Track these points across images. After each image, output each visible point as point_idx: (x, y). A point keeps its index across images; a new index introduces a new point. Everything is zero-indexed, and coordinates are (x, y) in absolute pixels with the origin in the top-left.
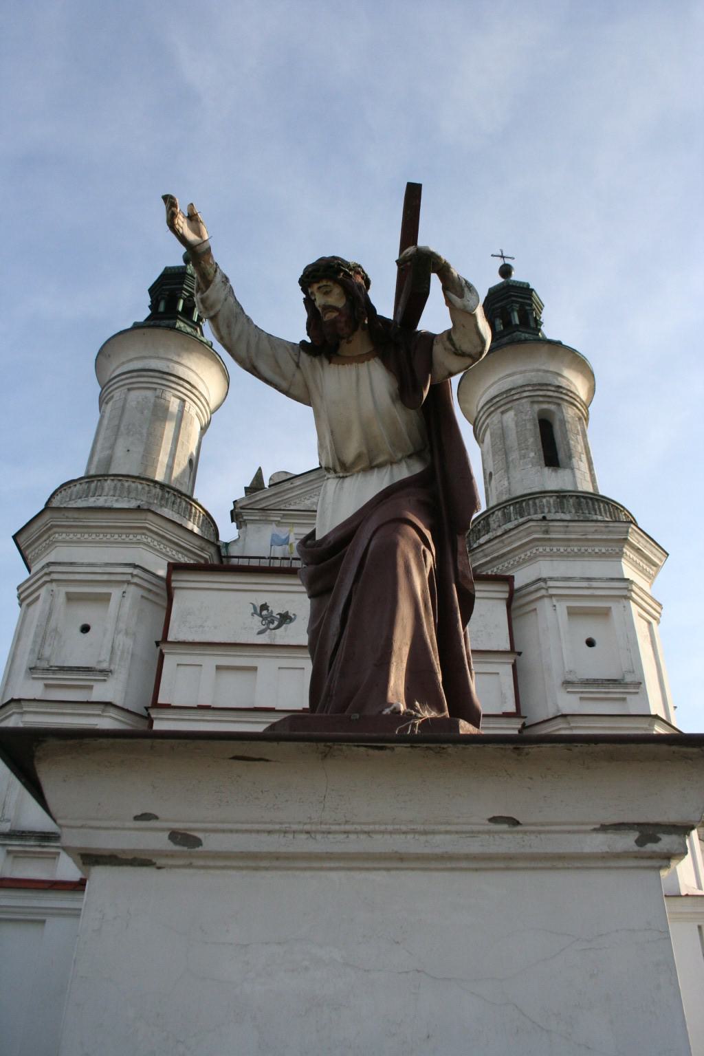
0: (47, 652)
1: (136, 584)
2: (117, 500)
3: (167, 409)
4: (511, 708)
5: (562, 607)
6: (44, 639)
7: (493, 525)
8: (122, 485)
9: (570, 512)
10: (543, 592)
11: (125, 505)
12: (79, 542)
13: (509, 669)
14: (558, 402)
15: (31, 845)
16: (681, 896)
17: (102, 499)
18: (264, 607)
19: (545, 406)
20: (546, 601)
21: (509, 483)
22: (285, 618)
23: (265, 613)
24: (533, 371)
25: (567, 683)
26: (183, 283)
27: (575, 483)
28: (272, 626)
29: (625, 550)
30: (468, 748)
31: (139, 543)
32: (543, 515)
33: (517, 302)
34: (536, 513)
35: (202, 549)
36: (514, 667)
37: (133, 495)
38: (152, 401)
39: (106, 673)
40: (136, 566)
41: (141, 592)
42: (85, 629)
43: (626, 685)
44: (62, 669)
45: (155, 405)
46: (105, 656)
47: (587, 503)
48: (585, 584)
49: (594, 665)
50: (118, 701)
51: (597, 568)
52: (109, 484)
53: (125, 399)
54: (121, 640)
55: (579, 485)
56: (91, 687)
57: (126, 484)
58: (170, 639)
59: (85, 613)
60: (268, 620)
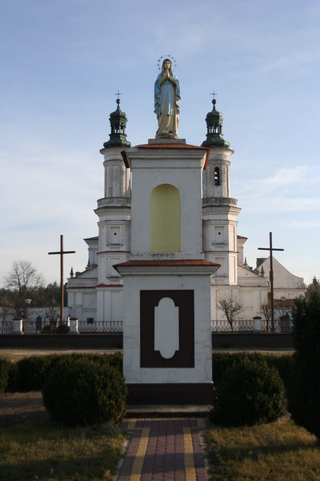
0: (109, 241)
1: (125, 224)
2: (118, 204)
3: (123, 171)
5: (213, 226)
6: (108, 238)
10: (210, 223)
12: (111, 214)
14: (221, 164)
15: (114, 279)
17: (114, 204)
19: (217, 166)
20: (210, 225)
21: (207, 188)
24: (215, 154)
25: (213, 244)
26: (119, 120)
27: (222, 195)
30: (177, 118)
31: (124, 214)
33: (214, 122)
34: (210, 203)
37: (121, 202)
39: (122, 245)
40: (124, 221)
42: (115, 234)
43: (225, 244)
44: (113, 245)
45: (120, 170)
46: (121, 241)
48: (219, 221)
49: (219, 239)
50: (125, 251)
51: (222, 217)
52: (115, 200)
53: (112, 169)
54: (124, 237)
55: (223, 195)
56: (119, 248)
57: (119, 199)
59: (115, 231)
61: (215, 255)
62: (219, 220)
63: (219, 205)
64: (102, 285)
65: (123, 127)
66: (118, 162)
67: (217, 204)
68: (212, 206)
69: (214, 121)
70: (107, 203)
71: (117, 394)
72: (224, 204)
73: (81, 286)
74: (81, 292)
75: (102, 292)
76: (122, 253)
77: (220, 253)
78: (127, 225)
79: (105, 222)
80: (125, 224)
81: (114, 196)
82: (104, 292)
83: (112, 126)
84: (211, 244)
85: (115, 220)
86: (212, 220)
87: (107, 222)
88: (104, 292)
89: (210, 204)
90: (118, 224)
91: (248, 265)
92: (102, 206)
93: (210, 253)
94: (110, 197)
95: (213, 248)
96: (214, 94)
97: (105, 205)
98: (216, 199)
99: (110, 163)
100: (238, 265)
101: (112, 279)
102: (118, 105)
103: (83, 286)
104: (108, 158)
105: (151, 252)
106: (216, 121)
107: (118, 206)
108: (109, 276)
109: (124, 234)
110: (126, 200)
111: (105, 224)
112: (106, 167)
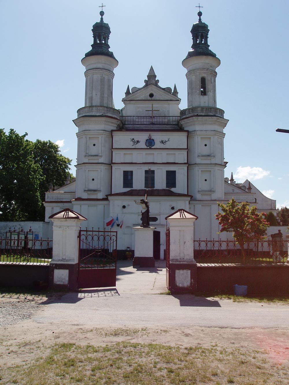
4: (186, 162)
5: (199, 138)
7: (186, 114)
8: (98, 109)
9: (204, 113)
11: (99, 115)
13: (186, 153)
15: (92, 192)
16: (104, 219)
18: (133, 139)
22: (138, 142)
23: (133, 140)
28: (135, 144)
29: (111, 251)
32: (197, 114)
33: (200, 32)
34: (196, 113)
35: (118, 122)
36: (187, 152)
38: (100, 78)
39: (101, 156)
41: (106, 136)
47: (209, 110)
48: (205, 132)
49: (205, 151)
52: (94, 108)
58: (113, 148)
60: (134, 142)
61: (201, 167)
62: (206, 131)
63: (205, 114)
64: (79, 199)
65: (206, 38)
66: (99, 70)
67: (203, 114)
68: (198, 116)
69: (200, 31)
70: (85, 113)
71: (186, 361)
72: (211, 114)
73: (59, 200)
74: (59, 206)
75: (79, 206)
76: (100, 165)
77: (206, 165)
78: (107, 135)
79: (83, 132)
80: (104, 134)
81: (94, 104)
82: (81, 206)
83: (94, 37)
84: (196, 155)
85: (94, 130)
86: (197, 131)
87: (85, 132)
88: (81, 206)
89: (196, 114)
90: (98, 133)
91: (234, 181)
92: (81, 115)
93: (196, 165)
94: (90, 105)
95: (198, 160)
96: (199, 7)
97: (84, 115)
98: (202, 108)
99: (91, 72)
100: (225, 181)
101: (89, 192)
102: (102, 17)
103: (61, 200)
104: (89, 68)
105: (124, 216)
106: (202, 31)
107: (98, 115)
108: (86, 189)
109: (103, 145)
110: (105, 109)
111: (83, 134)
112: (87, 76)
